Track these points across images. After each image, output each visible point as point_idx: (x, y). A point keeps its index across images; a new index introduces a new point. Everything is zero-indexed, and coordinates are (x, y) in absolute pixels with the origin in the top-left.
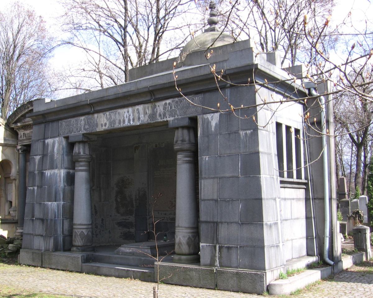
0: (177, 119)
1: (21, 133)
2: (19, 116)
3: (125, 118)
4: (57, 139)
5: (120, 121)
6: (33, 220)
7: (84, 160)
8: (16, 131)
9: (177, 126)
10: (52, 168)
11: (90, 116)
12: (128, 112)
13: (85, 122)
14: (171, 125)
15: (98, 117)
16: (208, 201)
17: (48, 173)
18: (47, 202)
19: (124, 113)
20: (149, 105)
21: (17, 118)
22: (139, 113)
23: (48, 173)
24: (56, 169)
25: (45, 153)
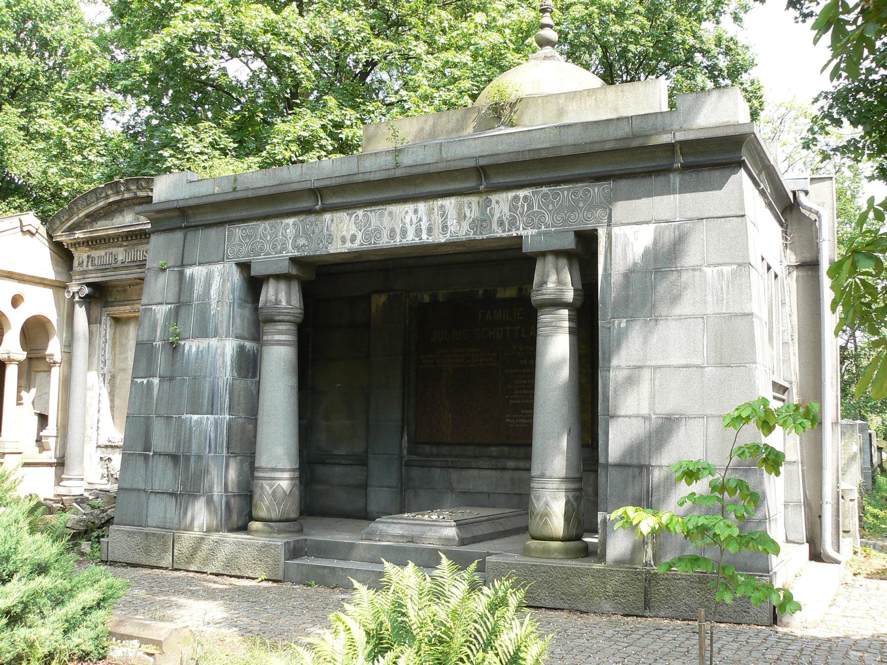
0: (545, 234)
1: (80, 255)
2: (81, 215)
3: (408, 226)
4: (217, 268)
5: (393, 230)
6: (146, 457)
8: (67, 249)
9: (543, 248)
10: (203, 333)
11: (312, 218)
12: (416, 211)
13: (298, 231)
14: (527, 248)
15: (332, 221)
17: (191, 346)
18: (188, 416)
19: (403, 214)
20: (474, 199)
21: (76, 218)
22: (444, 215)
23: (191, 347)
24: (215, 337)
25: (184, 299)
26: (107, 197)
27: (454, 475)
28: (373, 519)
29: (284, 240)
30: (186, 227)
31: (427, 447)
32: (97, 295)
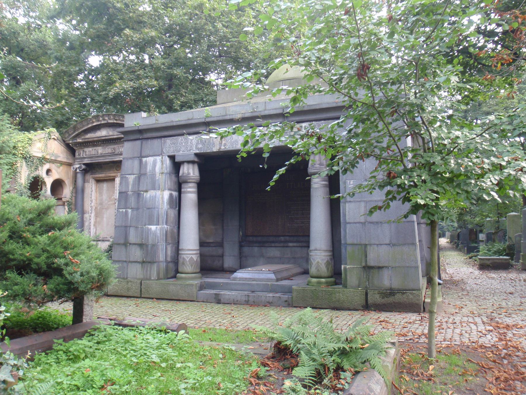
4: (159, 158)
7: (193, 181)
16: (354, 224)
25: (142, 172)
26: (93, 122)
27: (264, 250)
28: (235, 272)
29: (190, 146)
30: (142, 139)
31: (251, 238)
32: (88, 169)
